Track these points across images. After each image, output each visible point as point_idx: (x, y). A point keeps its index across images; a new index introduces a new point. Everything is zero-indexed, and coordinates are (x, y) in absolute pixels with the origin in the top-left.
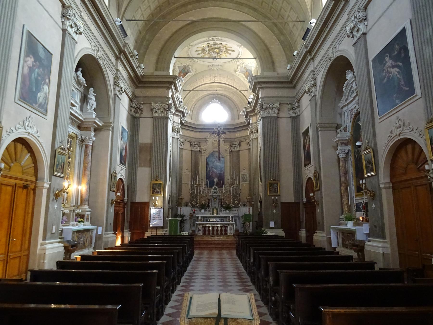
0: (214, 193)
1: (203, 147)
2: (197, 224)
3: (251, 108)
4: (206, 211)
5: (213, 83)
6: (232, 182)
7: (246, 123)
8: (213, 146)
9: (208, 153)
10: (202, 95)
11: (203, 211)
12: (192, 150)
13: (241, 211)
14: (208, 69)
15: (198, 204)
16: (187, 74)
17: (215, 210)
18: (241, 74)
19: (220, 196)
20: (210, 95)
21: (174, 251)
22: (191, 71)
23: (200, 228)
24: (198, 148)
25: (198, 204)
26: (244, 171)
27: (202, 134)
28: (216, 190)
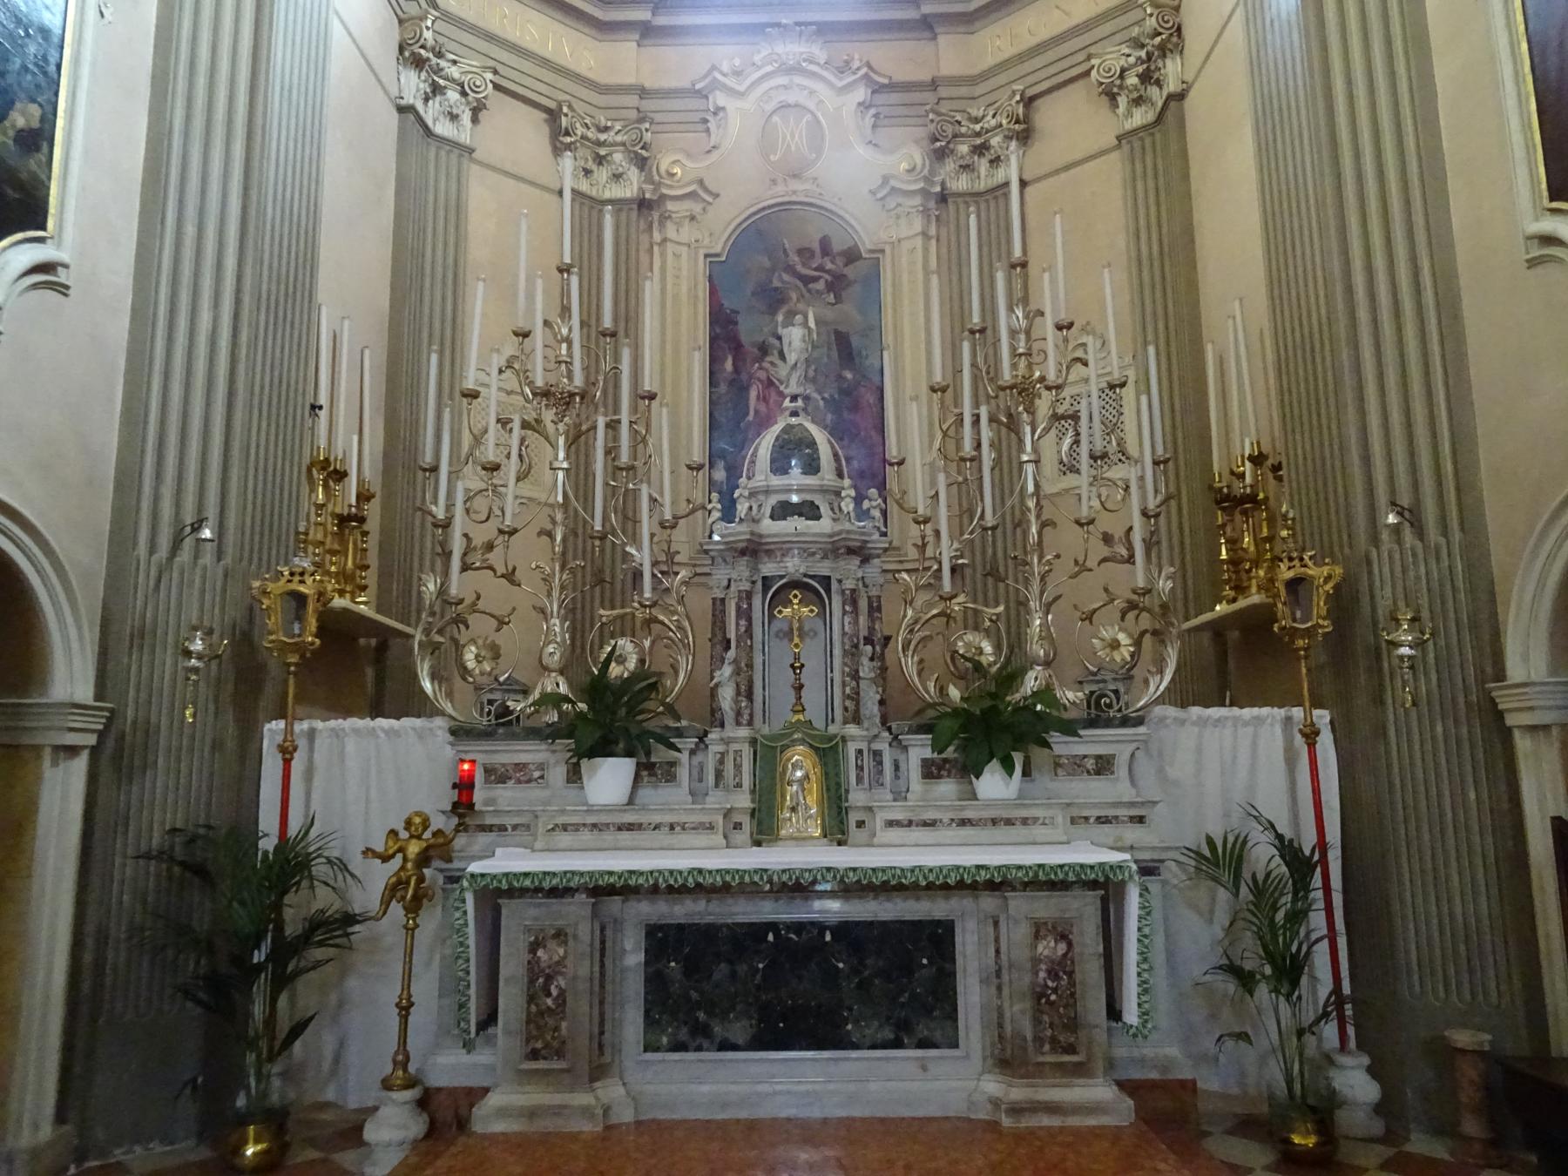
0: (784, 510)
4: (668, 773)
17: (800, 763)
19: (861, 552)
21: (1110, 311)
24: (633, 174)
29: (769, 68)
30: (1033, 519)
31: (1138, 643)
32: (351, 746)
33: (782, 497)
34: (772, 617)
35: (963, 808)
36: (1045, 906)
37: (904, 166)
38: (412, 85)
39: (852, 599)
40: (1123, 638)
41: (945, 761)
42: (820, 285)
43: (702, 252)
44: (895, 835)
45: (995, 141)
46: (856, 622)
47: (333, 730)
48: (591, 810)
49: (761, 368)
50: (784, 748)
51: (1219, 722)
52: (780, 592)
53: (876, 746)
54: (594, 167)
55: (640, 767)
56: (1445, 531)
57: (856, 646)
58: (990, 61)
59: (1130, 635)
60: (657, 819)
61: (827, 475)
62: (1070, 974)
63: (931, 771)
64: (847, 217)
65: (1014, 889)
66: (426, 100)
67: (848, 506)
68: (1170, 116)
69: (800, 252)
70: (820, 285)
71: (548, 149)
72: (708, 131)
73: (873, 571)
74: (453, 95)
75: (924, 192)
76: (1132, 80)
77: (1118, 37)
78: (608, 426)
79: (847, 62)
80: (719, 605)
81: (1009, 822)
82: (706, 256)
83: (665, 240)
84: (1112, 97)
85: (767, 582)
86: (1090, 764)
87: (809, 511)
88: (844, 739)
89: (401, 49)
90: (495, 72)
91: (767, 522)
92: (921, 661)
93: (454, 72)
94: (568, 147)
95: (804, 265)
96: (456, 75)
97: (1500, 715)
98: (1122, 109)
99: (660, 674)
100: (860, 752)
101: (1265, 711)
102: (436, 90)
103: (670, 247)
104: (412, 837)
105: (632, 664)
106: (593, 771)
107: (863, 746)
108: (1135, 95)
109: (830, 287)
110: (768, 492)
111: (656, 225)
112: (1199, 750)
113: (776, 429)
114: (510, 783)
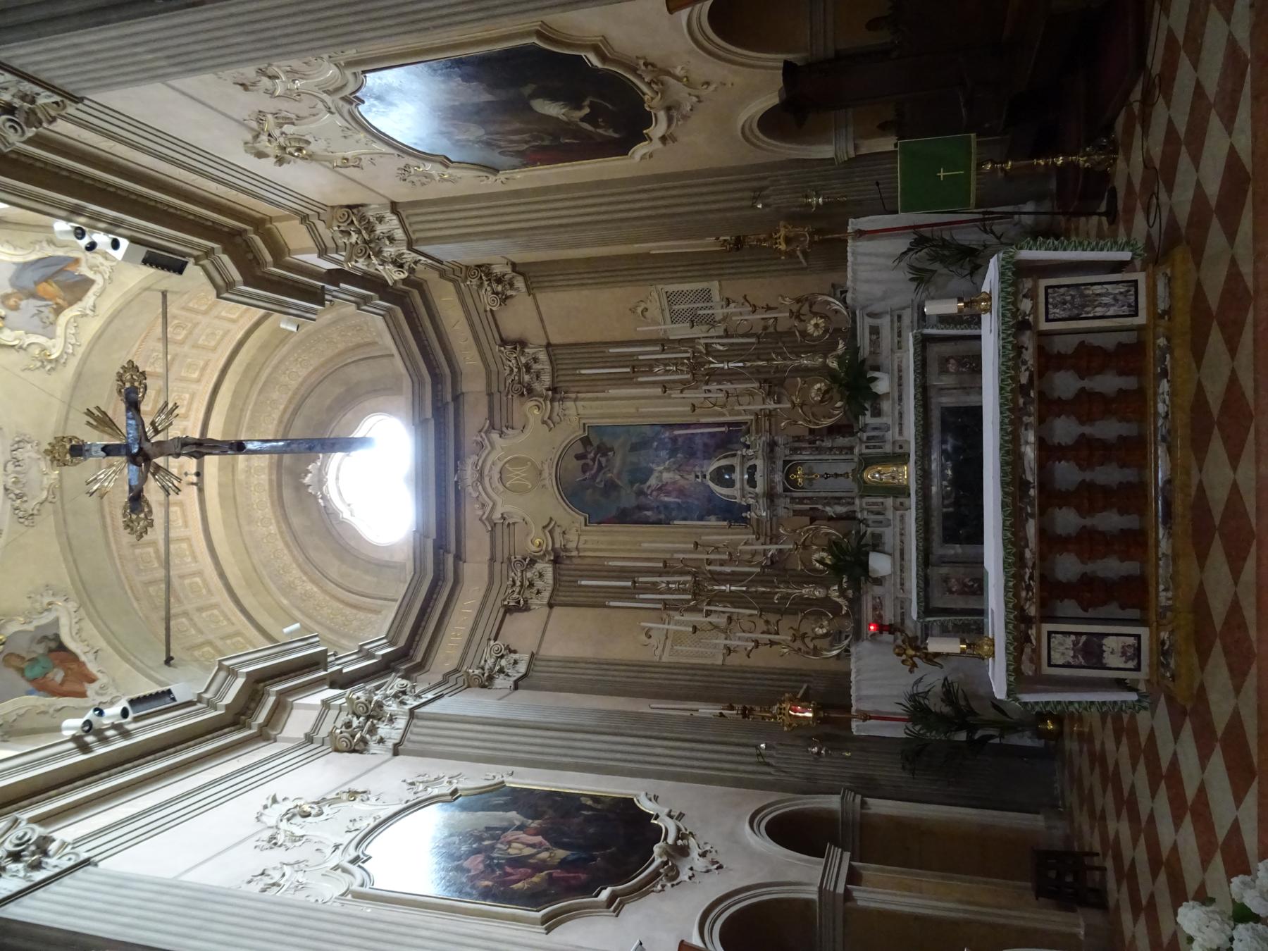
0: (752, 482)
1: (534, 541)
2: (1018, 680)
3: (209, 253)
4: (877, 538)
5: (201, 490)
6: (677, 362)
7: (388, 310)
8: (530, 490)
9: (571, 519)
10: (280, 545)
11: (880, 564)
12: (545, 601)
13: (878, 290)
14: (48, 523)
15: (834, 593)
16: (61, 647)
18: (60, 330)
19: (772, 445)
20: (282, 506)
22: (46, 619)
23: (1063, 650)
24: (539, 566)
25: (834, 593)
26: (654, 311)
27: (470, 545)
28: (731, 469)
29: (480, 487)
30: (755, 364)
31: (815, 314)
32: (864, 692)
33: (745, 482)
34: (802, 488)
35: (893, 399)
36: (933, 368)
37: (536, 412)
38: (500, 681)
39: (795, 450)
40: (813, 322)
41: (871, 406)
42: (603, 460)
43: (584, 528)
44: (905, 432)
45: (523, 360)
46: (805, 448)
47: (857, 701)
48: (894, 573)
49: (651, 494)
50: (865, 482)
51: (854, 272)
52: (791, 484)
53: (865, 439)
54: (535, 588)
55: (874, 550)
56: (765, 178)
57: (817, 448)
58: (479, 363)
59: (811, 319)
60: (898, 542)
61: (735, 461)
62: (963, 357)
63: (877, 413)
64: (564, 445)
65: (926, 382)
66: (508, 675)
67: (750, 452)
68: (521, 269)
69: (584, 472)
70: (603, 460)
71: (526, 614)
72: (514, 524)
73: (780, 440)
74: (503, 662)
75: (552, 400)
76: (500, 288)
77: (475, 295)
78: (709, 565)
79: (477, 443)
80: (797, 513)
81: (900, 378)
82: (586, 525)
83: (577, 549)
84: (507, 297)
85: (786, 490)
86: (874, 337)
87: (753, 469)
88: (861, 455)
89: (483, 686)
90: (489, 639)
91: (757, 490)
92: (824, 417)
93: (490, 662)
94: (526, 602)
95: (592, 469)
96: (493, 660)
97: (850, 159)
98: (513, 293)
99: (829, 540)
100: (867, 447)
101: (849, 249)
102: (501, 671)
103: (581, 546)
104: (905, 653)
105: (824, 554)
106: (875, 571)
107: (864, 446)
108: (508, 287)
109: (604, 455)
110: (742, 489)
111: (568, 554)
112: (867, 281)
113: (712, 485)
114: (882, 613)
